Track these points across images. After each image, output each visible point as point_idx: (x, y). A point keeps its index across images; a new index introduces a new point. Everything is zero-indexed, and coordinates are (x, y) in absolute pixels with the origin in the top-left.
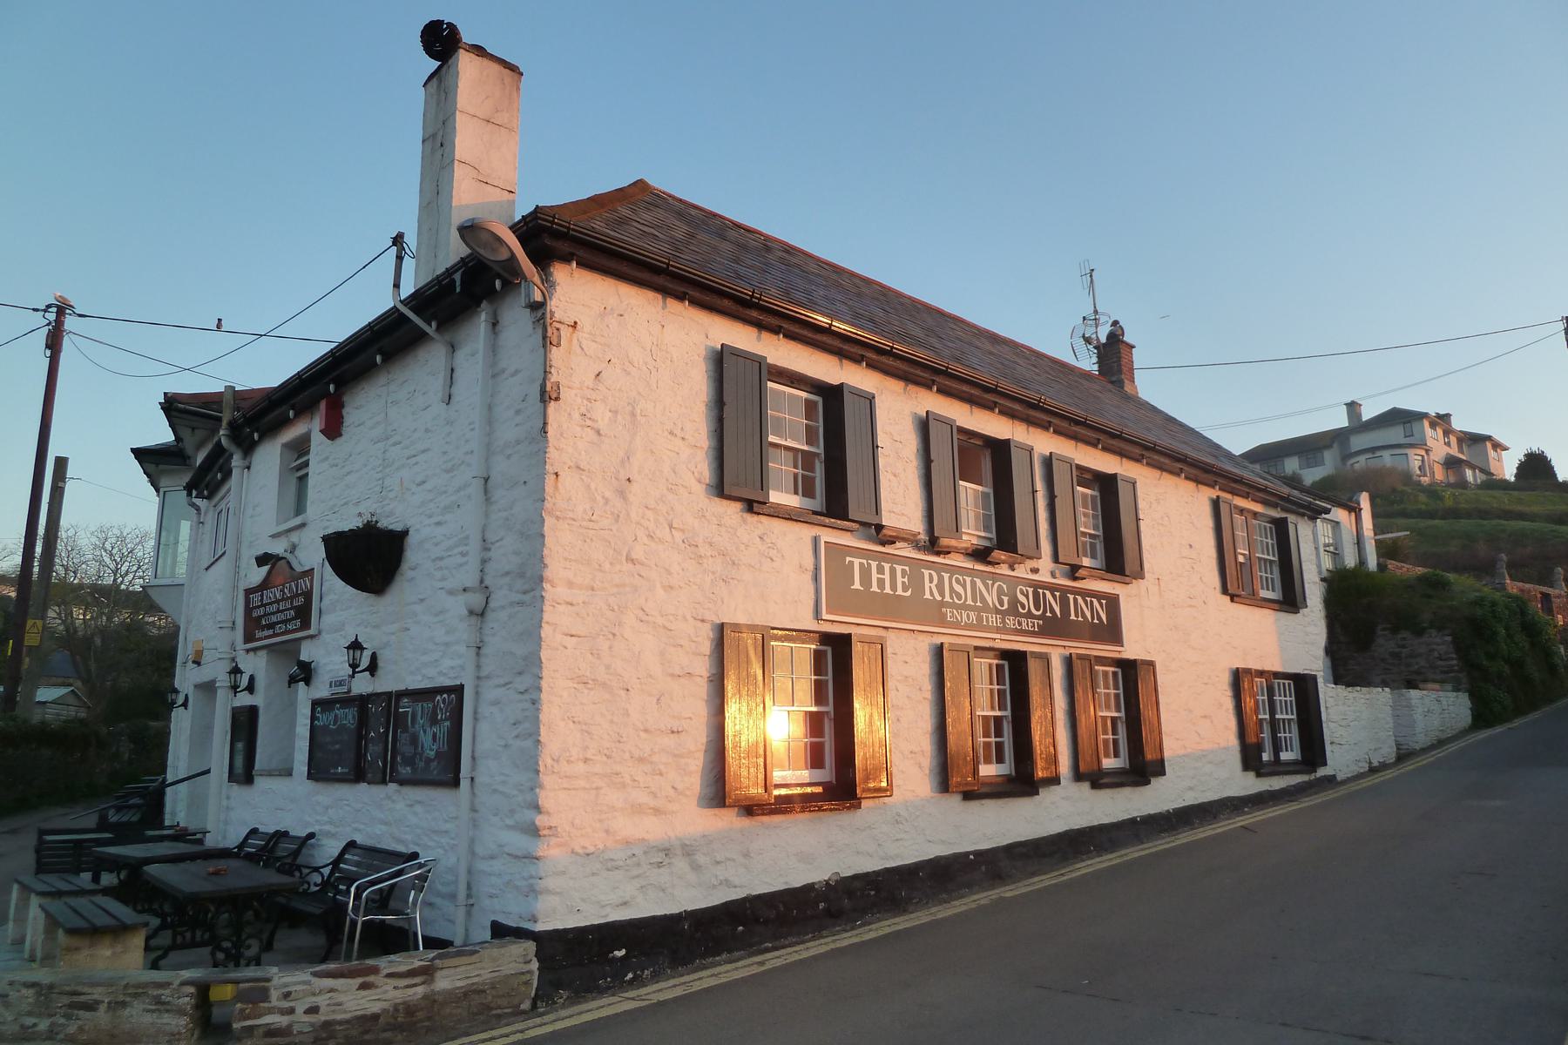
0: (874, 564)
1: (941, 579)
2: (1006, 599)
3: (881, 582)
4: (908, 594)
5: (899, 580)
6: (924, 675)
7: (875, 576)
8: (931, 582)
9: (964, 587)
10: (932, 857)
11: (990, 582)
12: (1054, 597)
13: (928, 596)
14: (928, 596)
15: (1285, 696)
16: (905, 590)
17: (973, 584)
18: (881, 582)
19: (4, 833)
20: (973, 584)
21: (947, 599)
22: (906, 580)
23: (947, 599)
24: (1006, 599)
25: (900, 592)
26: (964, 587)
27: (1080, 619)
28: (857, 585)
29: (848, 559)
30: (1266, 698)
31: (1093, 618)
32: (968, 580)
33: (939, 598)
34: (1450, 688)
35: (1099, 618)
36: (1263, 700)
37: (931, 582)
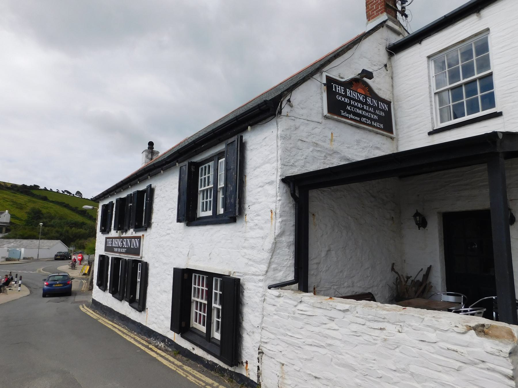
0: (337, 86)
1: (350, 92)
2: (364, 99)
3: (339, 90)
4: (344, 94)
5: (342, 90)
6: (358, 142)
7: (337, 88)
8: (348, 92)
9: (369, 100)
10: (484, 133)
11: (361, 95)
12: (376, 102)
13: (348, 95)
14: (348, 95)
15: (199, 285)
16: (343, 93)
17: (357, 94)
18: (339, 90)
19: (517, 123)
20: (357, 94)
21: (352, 97)
22: (343, 90)
23: (352, 97)
24: (364, 99)
25: (342, 93)
26: (369, 100)
27: (358, 99)
28: (334, 90)
29: (332, 84)
30: (214, 291)
31: (385, 109)
32: (356, 93)
33: (350, 96)
34: (101, 259)
35: (386, 109)
36: (216, 289)
37: (348, 92)
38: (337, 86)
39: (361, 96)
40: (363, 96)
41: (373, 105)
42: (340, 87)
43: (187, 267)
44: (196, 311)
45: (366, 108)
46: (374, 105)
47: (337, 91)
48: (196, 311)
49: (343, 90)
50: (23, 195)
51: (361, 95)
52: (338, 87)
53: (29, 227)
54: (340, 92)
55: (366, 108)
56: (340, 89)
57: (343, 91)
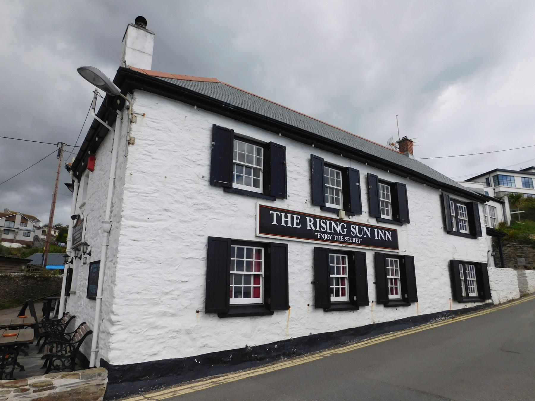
2: (345, 230)
3: (339, 239)
4: (299, 227)
9: (355, 229)
11: (338, 223)
20: (330, 224)
22: (298, 221)
24: (345, 230)
26: (355, 229)
33: (314, 229)
35: (388, 238)
38: (338, 236)
39: (339, 224)
40: (343, 225)
41: (364, 235)
42: (340, 237)
43: (387, 321)
44: (465, 225)
45: (355, 240)
46: (365, 236)
47: (338, 240)
48: (465, 225)
49: (297, 220)
50: (268, 366)
51: (338, 223)
52: (339, 237)
53: (529, 203)
54: (340, 240)
55: (355, 240)
56: (340, 238)
57: (297, 222)
